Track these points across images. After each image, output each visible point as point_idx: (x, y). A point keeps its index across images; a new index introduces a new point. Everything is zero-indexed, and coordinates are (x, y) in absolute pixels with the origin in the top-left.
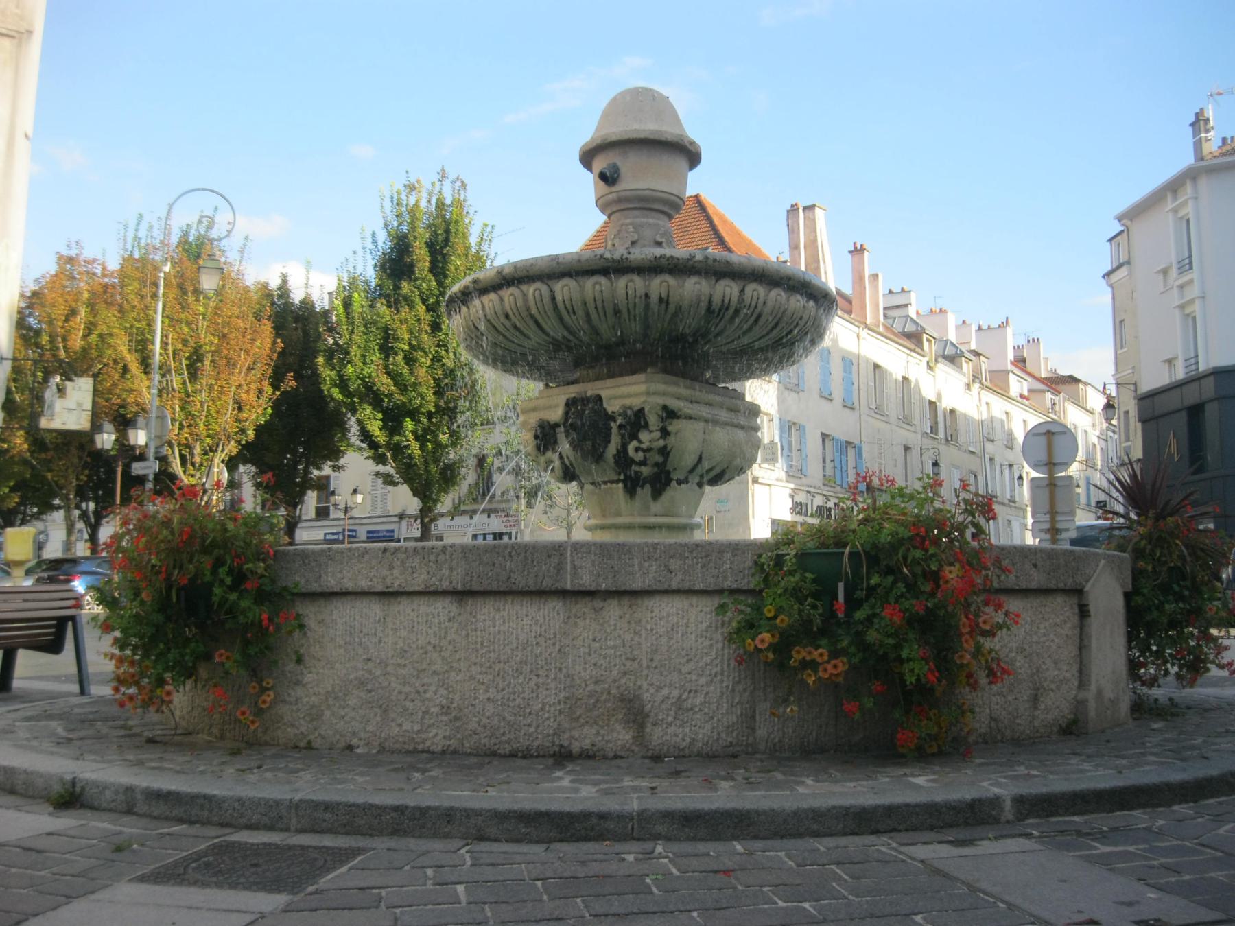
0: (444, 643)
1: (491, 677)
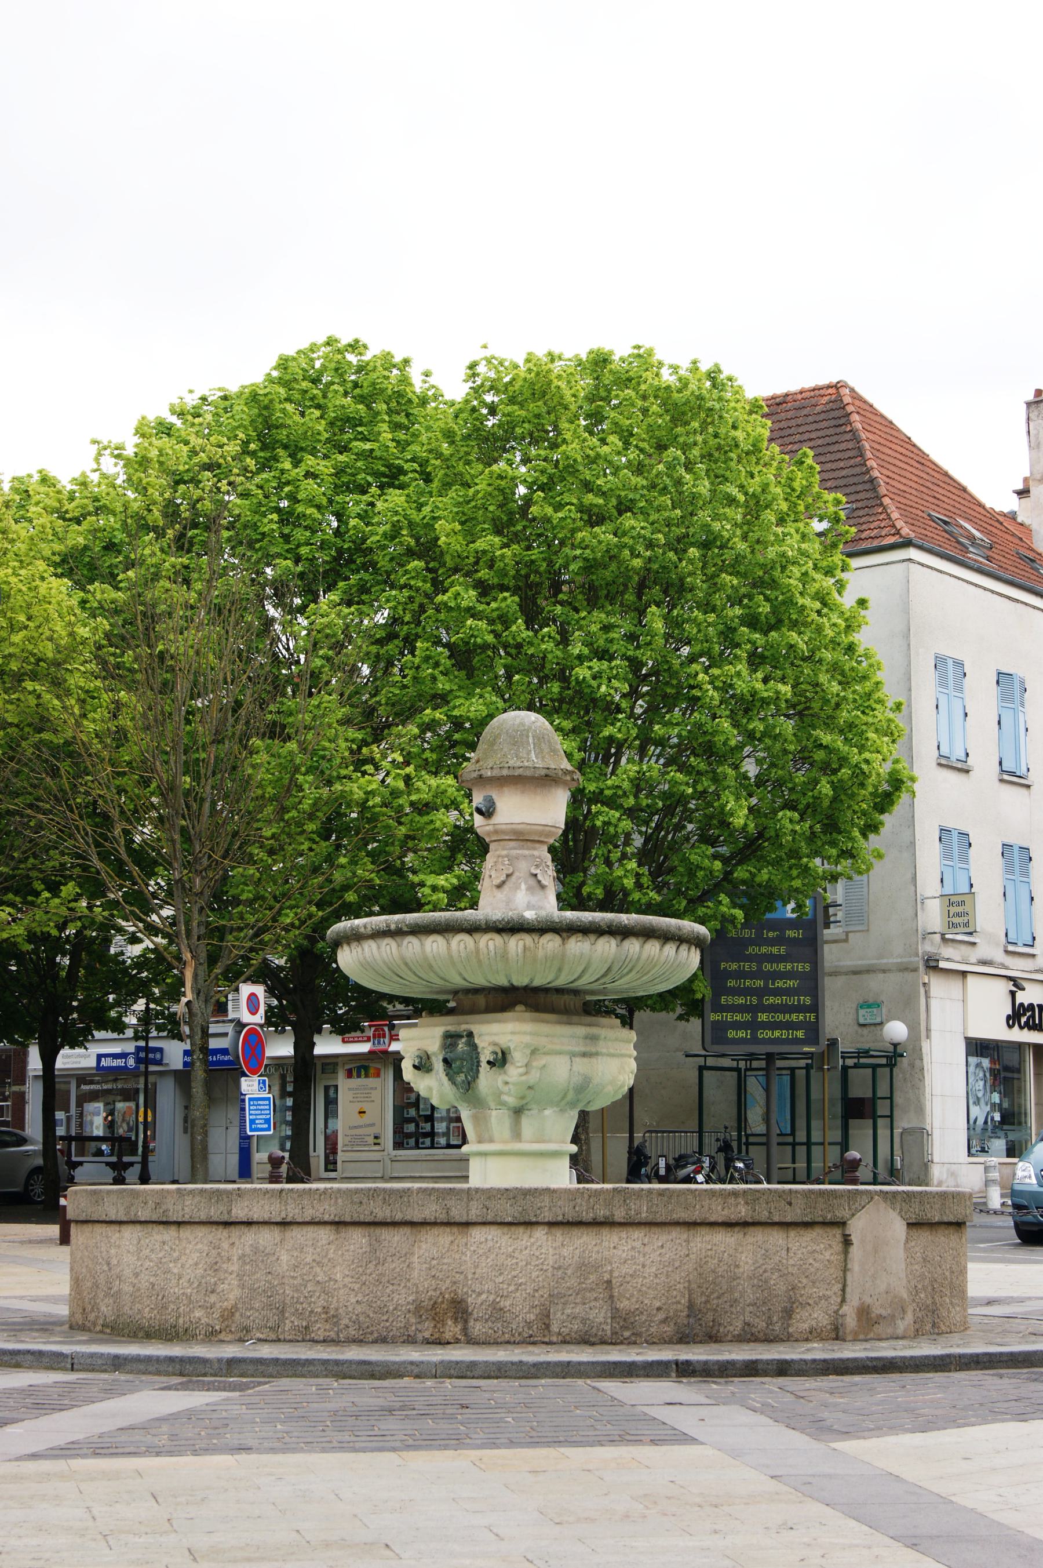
0: (325, 1261)
1: (358, 1285)
